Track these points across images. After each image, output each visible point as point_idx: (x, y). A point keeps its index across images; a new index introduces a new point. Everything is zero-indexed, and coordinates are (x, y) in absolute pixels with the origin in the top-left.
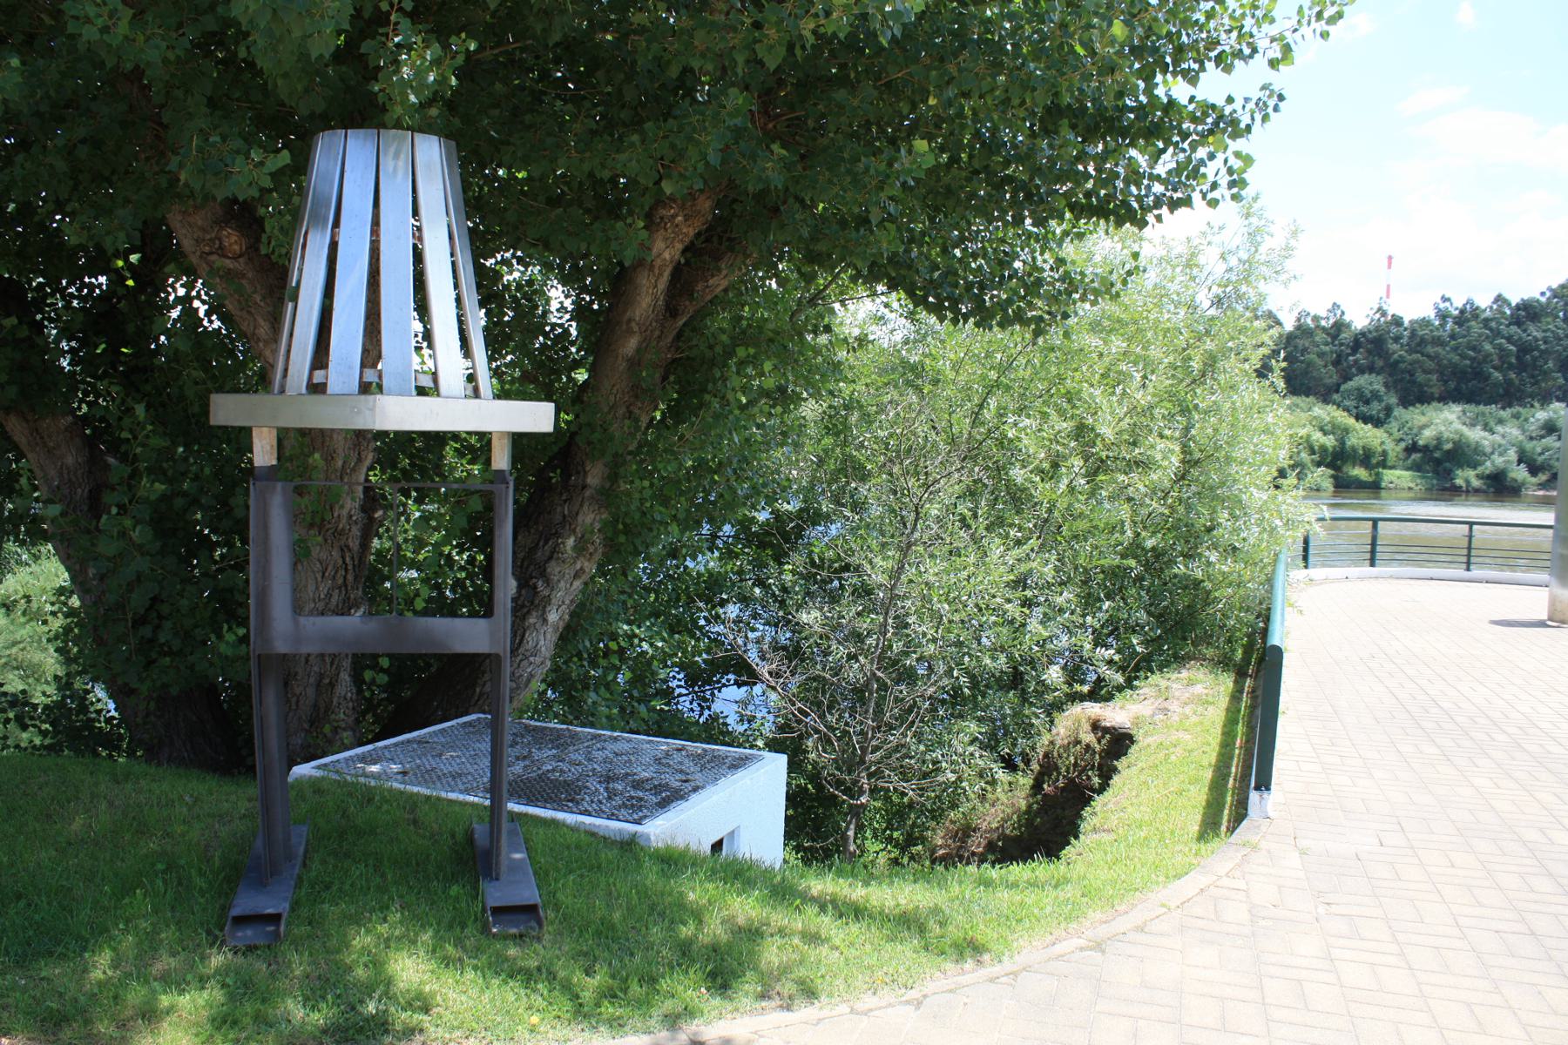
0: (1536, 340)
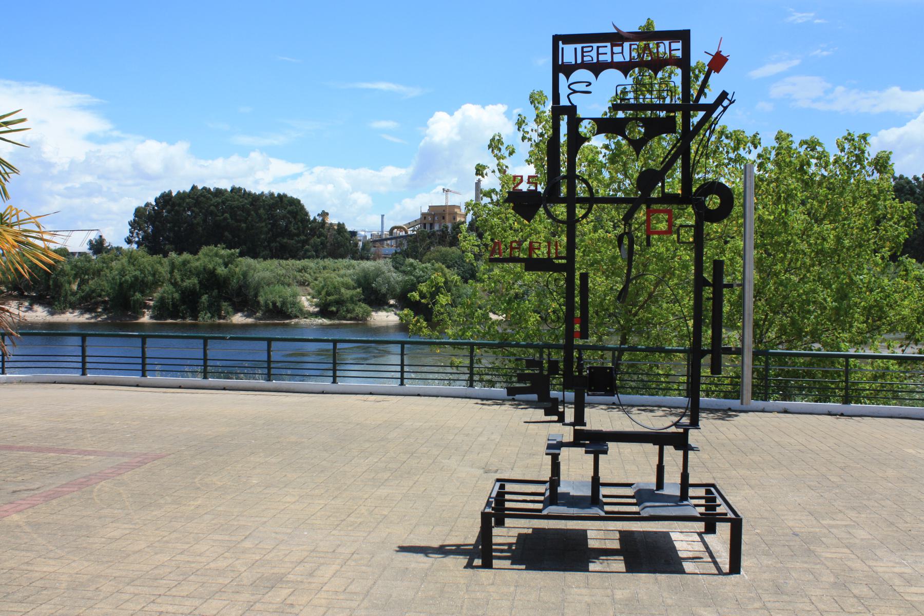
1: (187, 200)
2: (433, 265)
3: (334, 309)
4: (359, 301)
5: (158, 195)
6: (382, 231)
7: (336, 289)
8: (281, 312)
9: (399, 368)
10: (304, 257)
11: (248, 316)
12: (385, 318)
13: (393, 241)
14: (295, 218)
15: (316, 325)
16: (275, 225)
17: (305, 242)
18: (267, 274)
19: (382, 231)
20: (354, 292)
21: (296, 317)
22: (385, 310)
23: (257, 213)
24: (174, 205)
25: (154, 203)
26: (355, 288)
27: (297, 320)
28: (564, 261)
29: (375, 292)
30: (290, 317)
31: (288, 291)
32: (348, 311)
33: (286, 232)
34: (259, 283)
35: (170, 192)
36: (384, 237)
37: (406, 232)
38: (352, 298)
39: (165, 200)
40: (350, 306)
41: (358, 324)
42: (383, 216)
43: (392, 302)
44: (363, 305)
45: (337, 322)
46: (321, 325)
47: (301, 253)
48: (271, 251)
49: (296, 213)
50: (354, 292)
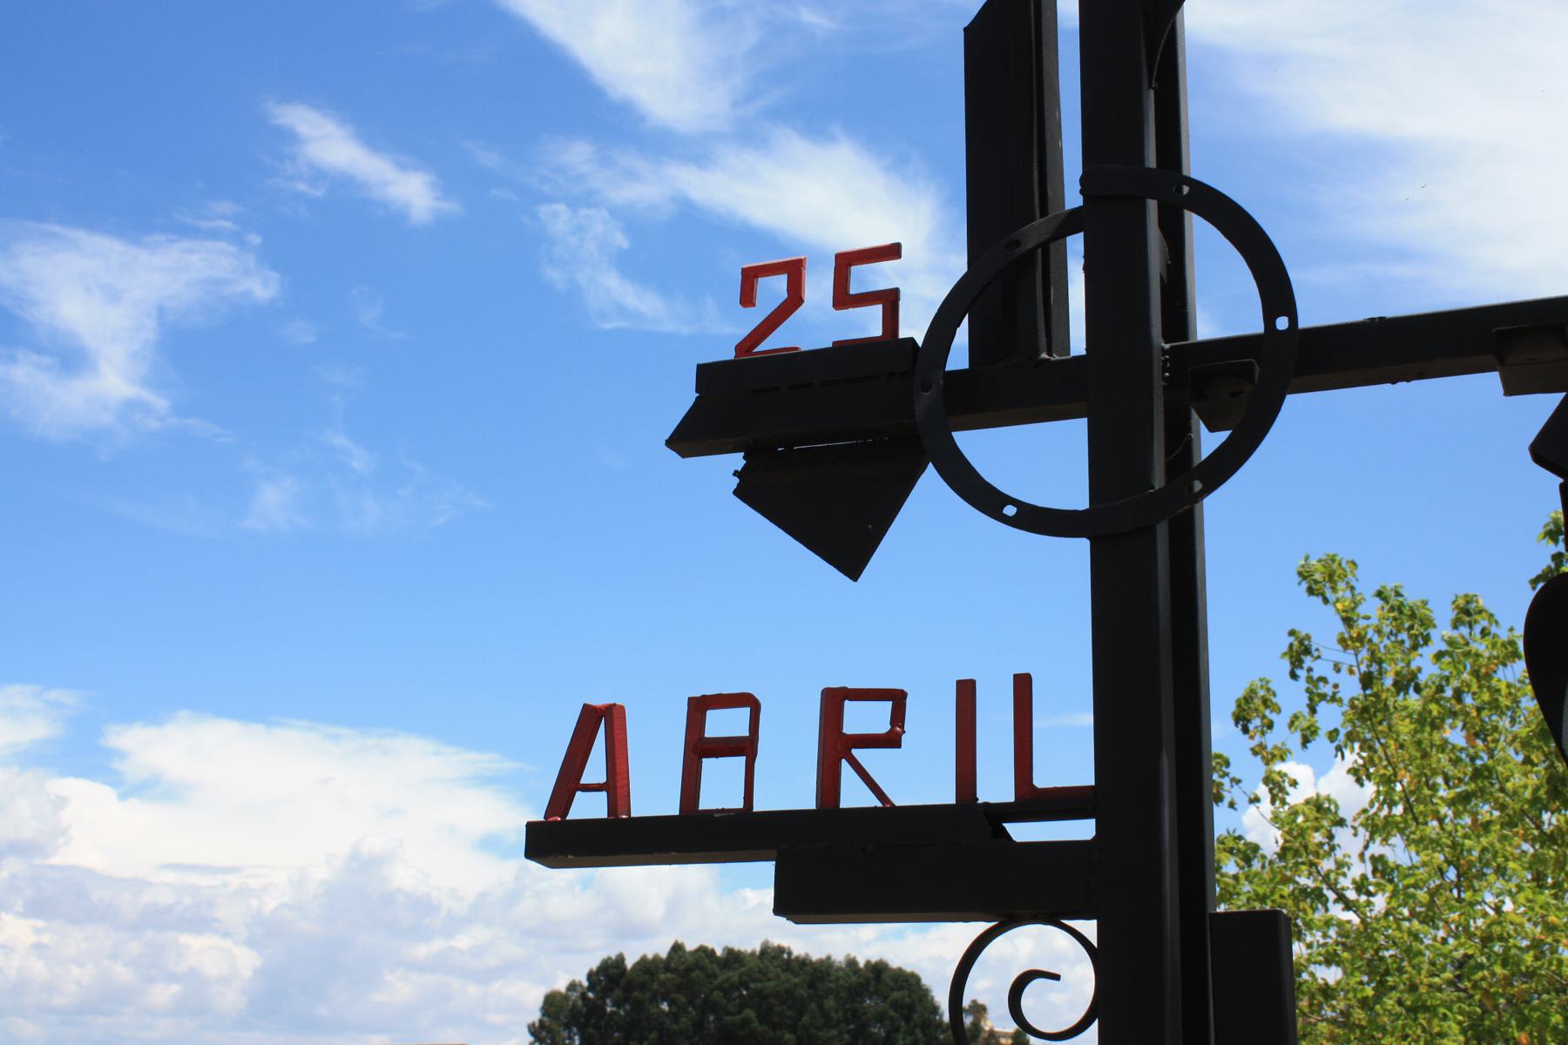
1: (662, 976)
5: (594, 964)
14: (908, 1019)
23: (821, 1006)
24: (629, 988)
25: (585, 984)
28: (1083, 830)
35: (620, 959)
39: (610, 975)
49: (911, 1008)
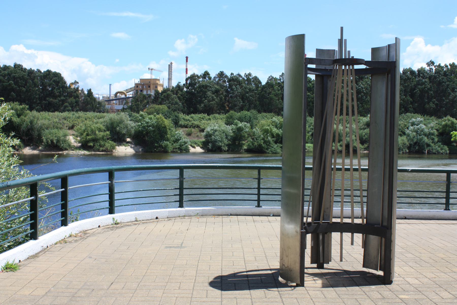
0: (362, 88)
2: (155, 116)
3: (91, 144)
4: (108, 139)
6: (110, 95)
7: (93, 132)
8: (56, 146)
9: (256, 191)
10: (64, 111)
11: (34, 149)
12: (125, 150)
13: (117, 101)
14: (57, 85)
15: (81, 155)
16: (44, 89)
17: (63, 102)
18: (46, 122)
19: (110, 95)
20: (105, 134)
21: (66, 149)
22: (124, 145)
26: (105, 131)
27: (67, 152)
29: (118, 133)
30: (62, 150)
31: (61, 133)
32: (101, 146)
33: (51, 94)
34: (41, 127)
36: (111, 98)
37: (126, 96)
38: (103, 136)
40: (102, 143)
41: (107, 154)
42: (110, 85)
43: (128, 140)
44: (110, 142)
45: (93, 153)
46: (84, 155)
47: (62, 108)
48: (42, 107)
50: (105, 134)
